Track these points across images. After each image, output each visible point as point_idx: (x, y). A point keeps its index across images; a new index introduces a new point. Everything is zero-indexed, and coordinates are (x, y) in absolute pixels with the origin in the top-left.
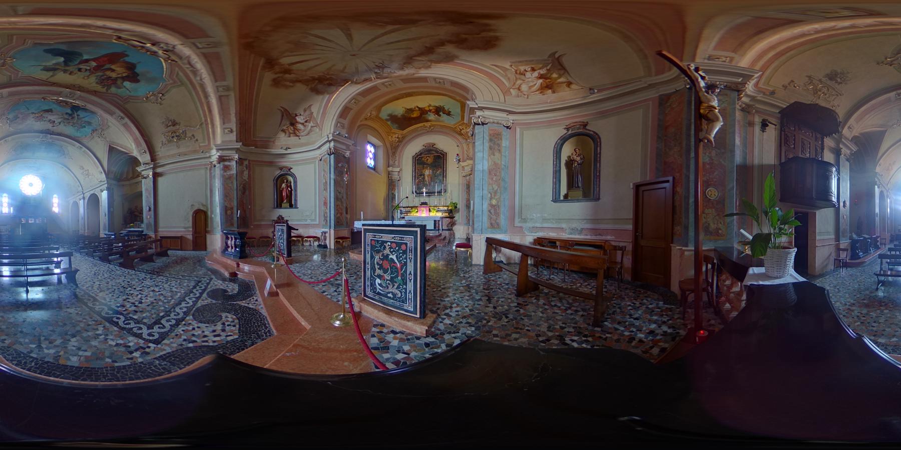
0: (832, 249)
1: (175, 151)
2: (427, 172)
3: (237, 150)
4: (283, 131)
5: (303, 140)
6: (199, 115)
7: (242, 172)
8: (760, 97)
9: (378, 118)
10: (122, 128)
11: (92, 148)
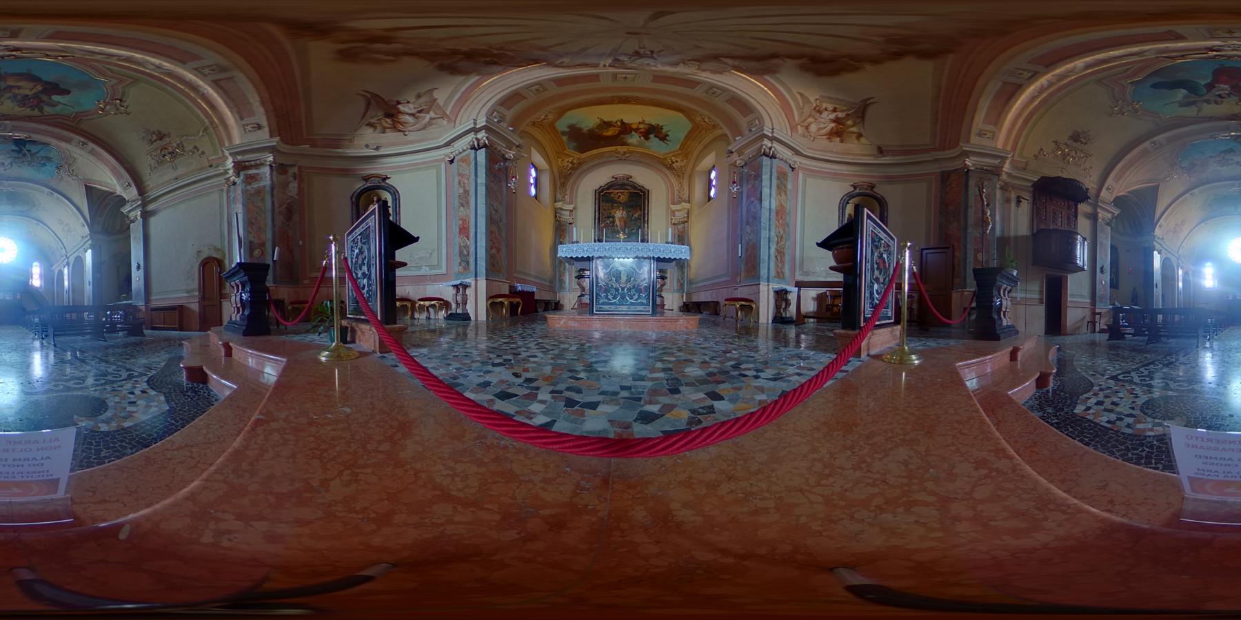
0: (1087, 313)
1: (171, 174)
2: (619, 214)
3: (272, 150)
4: (370, 125)
5: (412, 136)
6: (198, 117)
7: (285, 185)
8: (1015, 173)
9: (552, 126)
10: (92, 158)
11: (69, 195)
